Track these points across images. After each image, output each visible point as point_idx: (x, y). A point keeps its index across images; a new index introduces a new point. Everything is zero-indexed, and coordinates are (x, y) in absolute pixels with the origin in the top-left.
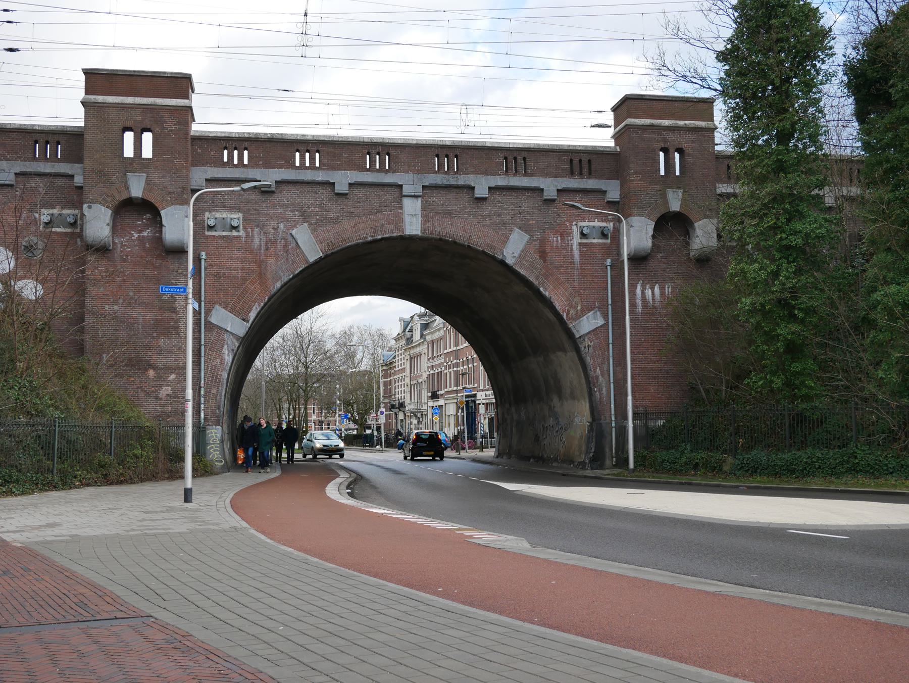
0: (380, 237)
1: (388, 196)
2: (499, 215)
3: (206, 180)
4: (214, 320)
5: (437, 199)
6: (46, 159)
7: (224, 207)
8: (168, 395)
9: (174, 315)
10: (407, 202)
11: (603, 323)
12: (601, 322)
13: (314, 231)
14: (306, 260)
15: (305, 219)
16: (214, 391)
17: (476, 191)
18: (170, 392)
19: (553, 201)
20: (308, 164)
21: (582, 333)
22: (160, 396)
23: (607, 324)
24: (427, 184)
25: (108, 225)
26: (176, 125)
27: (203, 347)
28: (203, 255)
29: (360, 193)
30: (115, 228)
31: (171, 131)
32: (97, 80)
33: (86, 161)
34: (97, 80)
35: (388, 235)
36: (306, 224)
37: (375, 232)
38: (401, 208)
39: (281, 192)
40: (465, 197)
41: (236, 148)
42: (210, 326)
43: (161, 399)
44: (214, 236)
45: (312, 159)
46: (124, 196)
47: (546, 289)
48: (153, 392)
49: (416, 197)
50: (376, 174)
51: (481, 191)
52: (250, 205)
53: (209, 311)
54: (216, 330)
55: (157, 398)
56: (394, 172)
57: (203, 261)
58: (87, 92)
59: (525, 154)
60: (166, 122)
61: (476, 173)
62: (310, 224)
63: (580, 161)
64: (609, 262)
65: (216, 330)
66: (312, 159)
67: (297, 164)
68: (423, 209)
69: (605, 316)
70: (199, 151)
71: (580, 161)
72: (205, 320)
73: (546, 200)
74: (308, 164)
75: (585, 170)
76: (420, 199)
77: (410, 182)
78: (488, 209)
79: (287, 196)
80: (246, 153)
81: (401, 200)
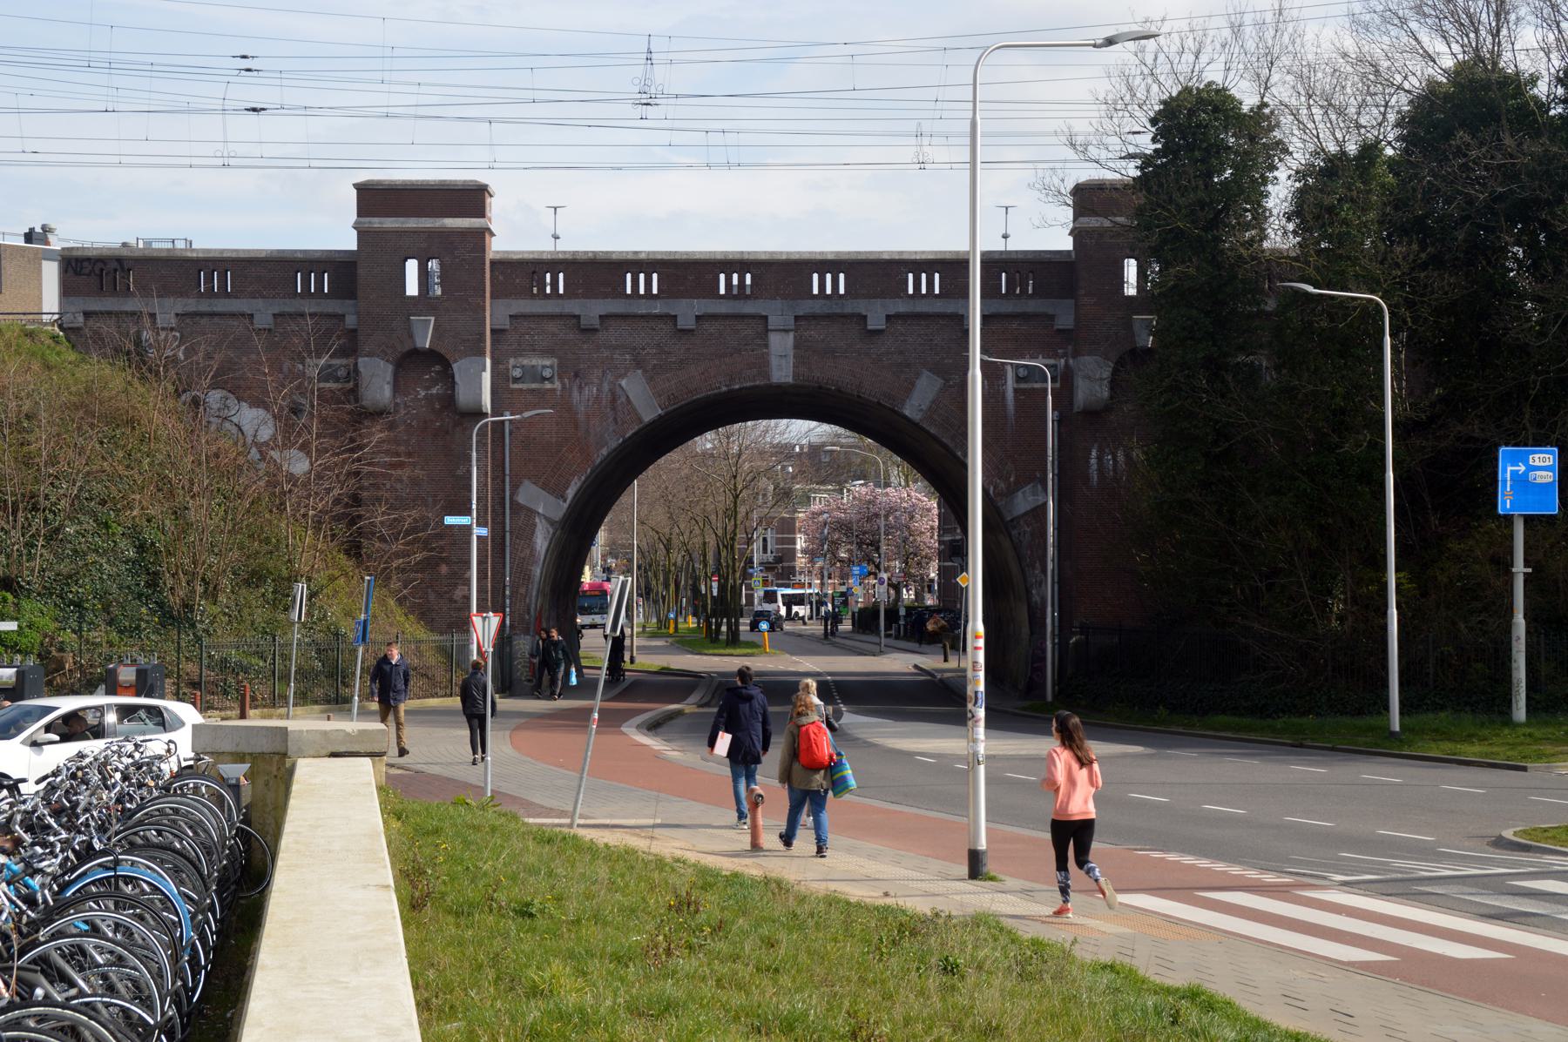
2: (901, 353)
4: (521, 499)
10: (774, 339)
13: (650, 380)
16: (522, 591)
29: (711, 328)
38: (766, 346)
42: (517, 508)
49: (786, 331)
51: (876, 322)
53: (515, 488)
55: (451, 600)
67: (629, 291)
68: (796, 347)
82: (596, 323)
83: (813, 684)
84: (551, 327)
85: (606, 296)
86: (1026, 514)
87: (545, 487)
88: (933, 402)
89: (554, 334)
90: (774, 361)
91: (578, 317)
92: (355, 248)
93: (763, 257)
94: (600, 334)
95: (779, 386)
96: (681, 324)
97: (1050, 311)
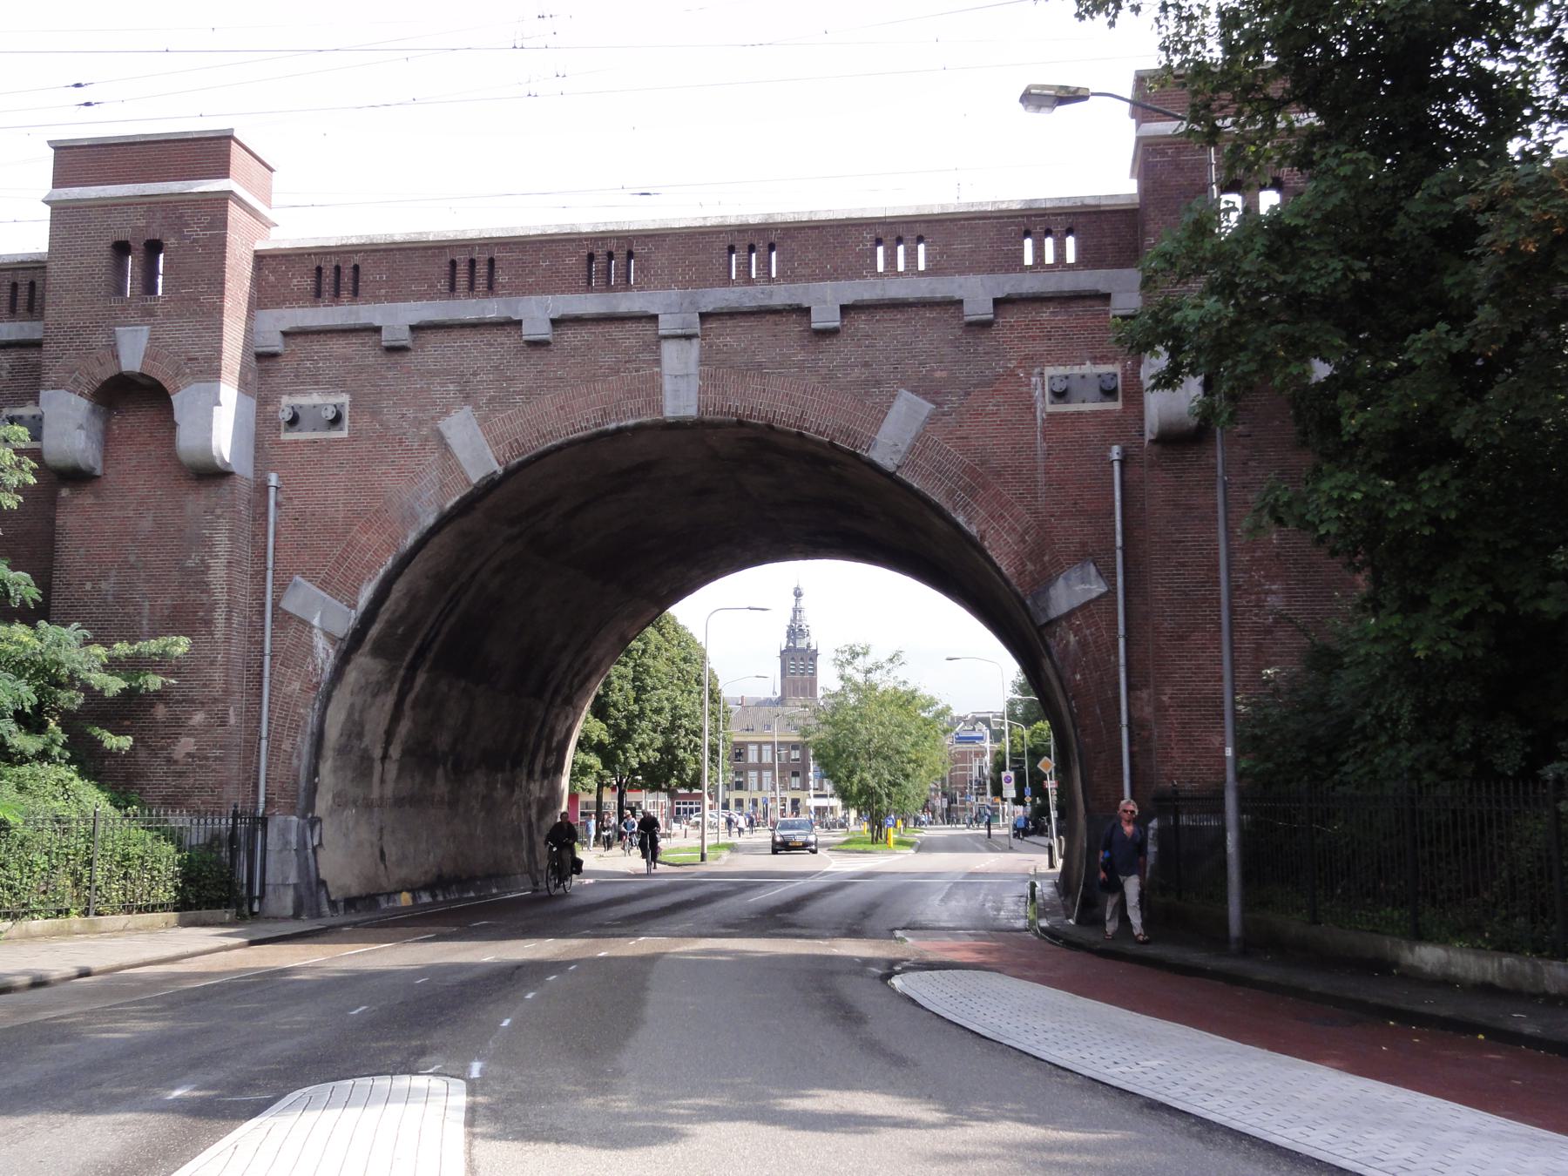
0: (612, 426)
1: (627, 336)
2: (866, 365)
3: (285, 334)
4: (289, 604)
5: (731, 337)
6: (749, 281)
7: (317, 383)
8: (188, 755)
9: (204, 597)
10: (669, 350)
11: (1103, 589)
12: (1098, 588)
13: (483, 421)
14: (468, 483)
15: (467, 398)
16: (286, 746)
17: (967, 308)
18: (192, 749)
19: (834, 332)
20: (901, 267)
21: (1053, 614)
22: (175, 757)
23: (1111, 593)
24: (710, 309)
25: (80, 427)
26: (206, 229)
27: (267, 659)
28: (273, 479)
29: (571, 336)
30: (107, 441)
31: (196, 240)
32: (74, 161)
33: (50, 312)
34: (74, 161)
35: (631, 422)
36: (468, 408)
37: (605, 414)
38: (658, 362)
39: (422, 347)
40: (793, 327)
41: (1048, 233)
42: (283, 618)
43: (176, 762)
44: (296, 442)
45: (911, 256)
46: (111, 372)
47: (415, 517)
48: (162, 748)
49: (688, 337)
50: (1069, 276)
51: (536, 324)
52: (364, 376)
53: (281, 587)
54: (294, 624)
55: (170, 761)
56: (642, 289)
57: (272, 491)
58: (58, 182)
59: (357, 259)
60: (187, 225)
61: (813, 278)
62: (477, 407)
63: (338, 268)
64: (1115, 452)
65: (294, 624)
66: (911, 256)
67: (881, 268)
68: (702, 362)
69: (1107, 574)
70: (272, 278)
71: (338, 268)
72: (275, 606)
73: (970, 324)
74: (901, 267)
75: (481, 282)
76: (695, 341)
77: (668, 304)
78: (832, 355)
79: (433, 351)
80: (921, 248)
81: (659, 347)
82: (404, 337)
83: (1233, 947)
84: (338, 346)
85: (420, 297)
86: (1070, 614)
87: (324, 585)
88: (918, 438)
89: (347, 359)
90: (668, 385)
91: (378, 330)
92: (44, 248)
93: (1049, 205)
94: (410, 356)
95: (678, 426)
96: (387, 338)
97: (1103, 288)
